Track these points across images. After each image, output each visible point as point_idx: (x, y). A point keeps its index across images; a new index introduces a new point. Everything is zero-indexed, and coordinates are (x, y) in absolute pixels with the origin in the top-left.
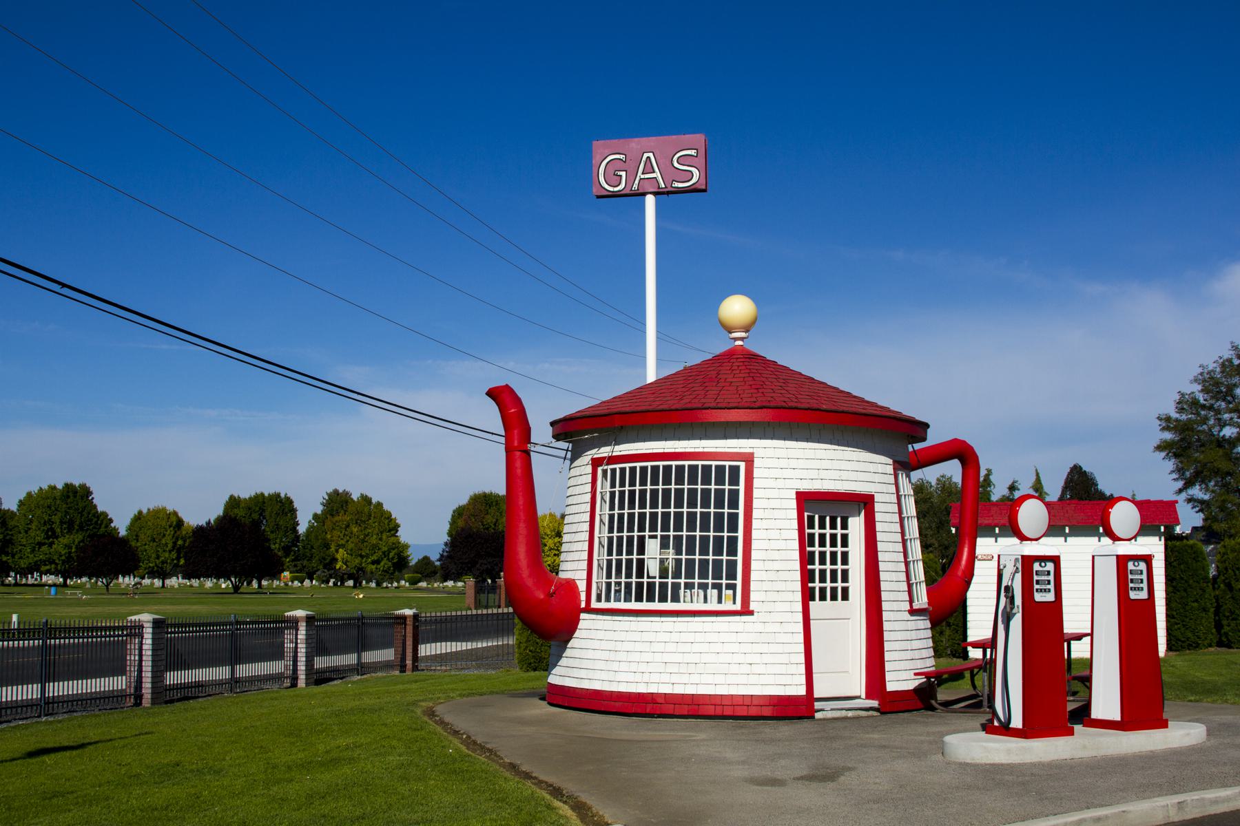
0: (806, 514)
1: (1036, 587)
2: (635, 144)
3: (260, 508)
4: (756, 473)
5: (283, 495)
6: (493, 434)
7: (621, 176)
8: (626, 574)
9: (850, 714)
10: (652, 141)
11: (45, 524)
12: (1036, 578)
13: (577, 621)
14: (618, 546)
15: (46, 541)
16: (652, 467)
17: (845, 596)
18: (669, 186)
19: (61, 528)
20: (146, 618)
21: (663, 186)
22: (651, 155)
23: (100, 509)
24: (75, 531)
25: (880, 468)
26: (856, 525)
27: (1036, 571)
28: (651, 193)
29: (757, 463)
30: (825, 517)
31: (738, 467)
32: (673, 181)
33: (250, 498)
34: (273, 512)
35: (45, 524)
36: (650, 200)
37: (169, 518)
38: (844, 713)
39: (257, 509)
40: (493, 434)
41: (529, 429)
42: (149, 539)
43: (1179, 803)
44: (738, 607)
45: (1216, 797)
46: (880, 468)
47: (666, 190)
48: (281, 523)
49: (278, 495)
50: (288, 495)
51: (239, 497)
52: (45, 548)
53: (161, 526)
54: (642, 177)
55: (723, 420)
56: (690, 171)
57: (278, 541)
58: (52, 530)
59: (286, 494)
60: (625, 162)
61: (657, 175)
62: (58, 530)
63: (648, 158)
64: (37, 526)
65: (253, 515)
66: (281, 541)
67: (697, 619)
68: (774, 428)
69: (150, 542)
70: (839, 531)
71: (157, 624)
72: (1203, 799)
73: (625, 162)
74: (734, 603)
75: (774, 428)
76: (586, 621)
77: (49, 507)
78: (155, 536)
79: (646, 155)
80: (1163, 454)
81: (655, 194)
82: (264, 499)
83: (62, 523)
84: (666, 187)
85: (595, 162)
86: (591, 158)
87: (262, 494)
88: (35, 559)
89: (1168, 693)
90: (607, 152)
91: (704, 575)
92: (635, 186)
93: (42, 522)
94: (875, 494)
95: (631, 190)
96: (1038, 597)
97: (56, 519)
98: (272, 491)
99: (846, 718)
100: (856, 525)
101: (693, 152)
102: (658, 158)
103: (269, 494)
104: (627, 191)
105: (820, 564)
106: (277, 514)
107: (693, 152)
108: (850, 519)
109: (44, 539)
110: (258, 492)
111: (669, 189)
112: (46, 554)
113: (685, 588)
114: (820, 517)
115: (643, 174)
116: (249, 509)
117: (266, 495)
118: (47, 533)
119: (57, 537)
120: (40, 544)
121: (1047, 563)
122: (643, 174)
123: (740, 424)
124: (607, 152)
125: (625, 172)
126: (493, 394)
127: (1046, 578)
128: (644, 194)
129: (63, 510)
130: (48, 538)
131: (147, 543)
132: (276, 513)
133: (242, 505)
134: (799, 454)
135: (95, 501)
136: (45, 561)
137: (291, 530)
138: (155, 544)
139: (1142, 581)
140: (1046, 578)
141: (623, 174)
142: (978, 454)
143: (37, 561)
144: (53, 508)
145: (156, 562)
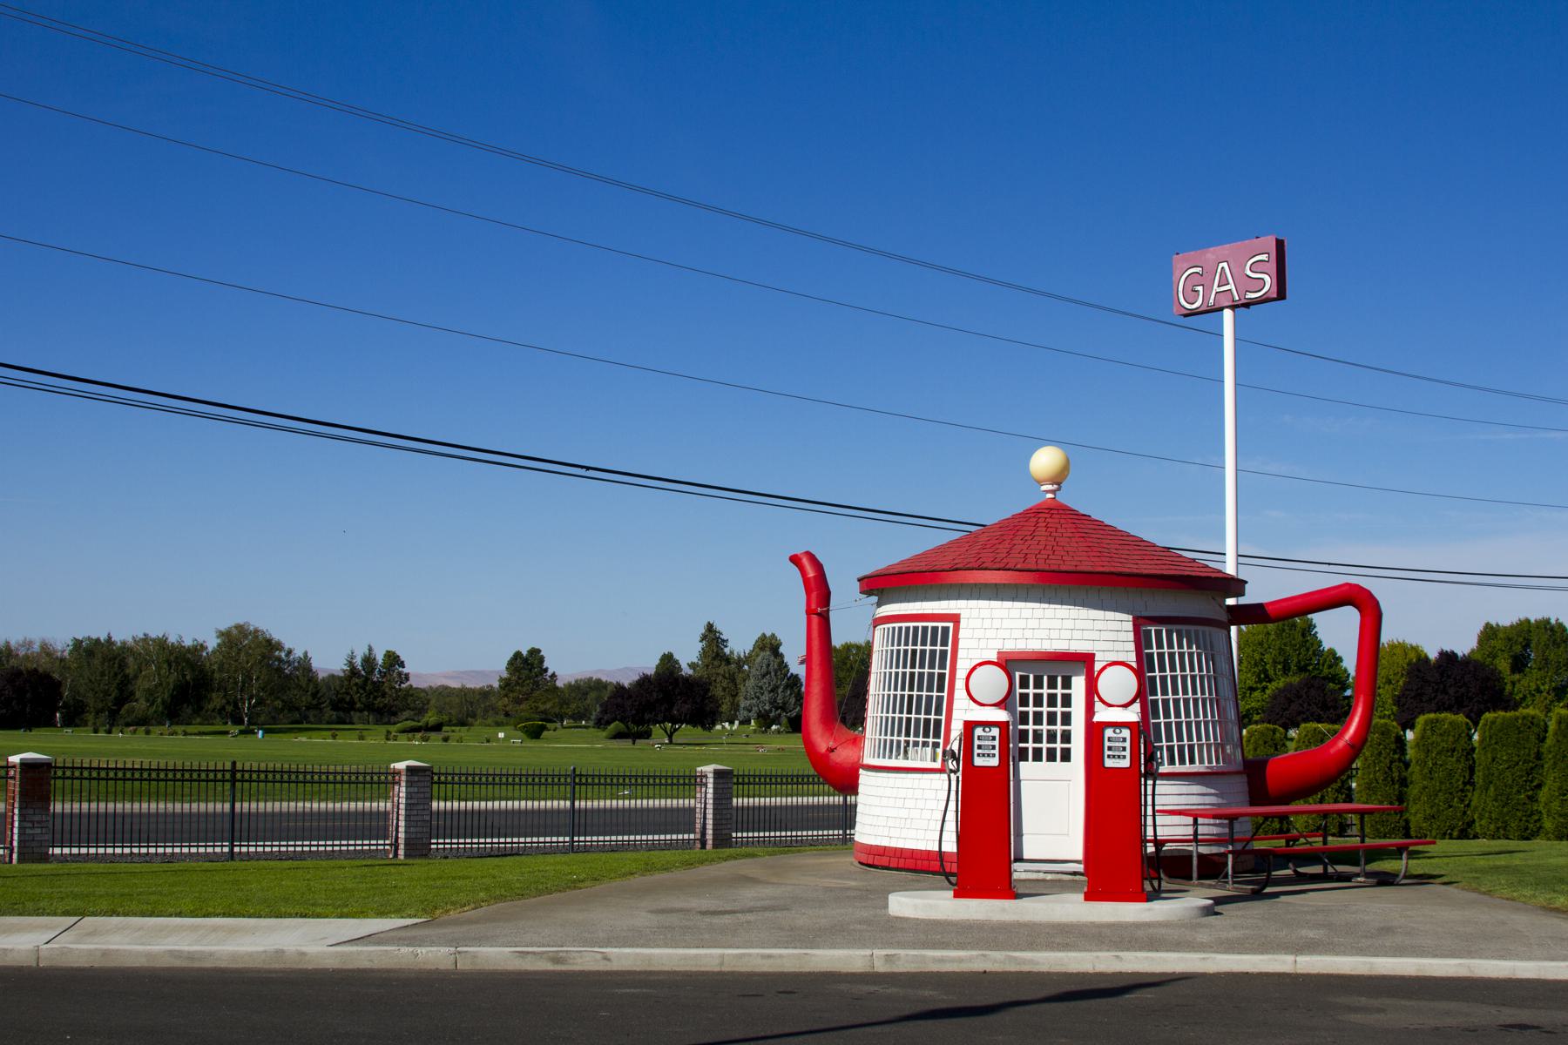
0: (1017, 674)
1: (1107, 752)
2: (1210, 255)
3: (1524, 639)
4: (962, 634)
5: (1553, 621)
6: (1329, 564)
7: (1198, 291)
8: (923, 733)
9: (1049, 877)
10: (1225, 249)
11: (1256, 665)
12: (1107, 744)
13: (857, 777)
14: (926, 704)
15: (1258, 685)
16: (943, 627)
17: (1066, 756)
18: (1242, 298)
19: (1275, 670)
20: (709, 769)
21: (1237, 299)
22: (1225, 265)
23: (1326, 646)
24: (1291, 673)
25: (1117, 626)
26: (1079, 684)
27: (979, 737)
28: (1227, 307)
29: (963, 623)
30: (1056, 677)
31: (948, 628)
32: (1247, 291)
33: (1512, 626)
34: (1540, 643)
35: (1256, 665)
36: (1228, 314)
37: (1406, 654)
38: (1041, 876)
39: (1521, 639)
40: (1329, 564)
41: (829, 593)
42: (1384, 680)
43: (887, 955)
44: (938, 765)
45: (942, 956)
46: (1117, 626)
47: (1241, 302)
48: (1552, 657)
49: (1548, 621)
50: (1560, 621)
51: (1497, 625)
52: (1257, 694)
53: (1398, 664)
54: (1218, 290)
55: (972, 582)
56: (1263, 279)
57: (1547, 680)
58: (1265, 671)
59: (1558, 620)
60: (1202, 275)
61: (1231, 286)
62: (1271, 672)
63: (1223, 268)
64: (1247, 668)
65: (1514, 648)
66: (1551, 681)
67: (910, 776)
68: (980, 589)
69: (1384, 684)
70: (1059, 691)
71: (717, 774)
72: (924, 956)
73: (1202, 275)
74: (934, 761)
75: (980, 589)
76: (865, 778)
77: (1261, 644)
78: (1391, 677)
79: (1221, 265)
80: (358, 661)
81: (1233, 307)
82: (1530, 627)
83: (1275, 662)
84: (1240, 300)
85: (1175, 279)
86: (1171, 274)
87: (1528, 621)
88: (1247, 707)
89: (955, 859)
90: (1186, 265)
91: (926, 735)
92: (1212, 301)
93: (1253, 662)
94: (1096, 653)
95: (1233, 301)
96: (978, 762)
97: (1267, 658)
98: (1539, 617)
99: (1044, 880)
100: (1079, 684)
101: (1264, 257)
102: (1233, 271)
103: (1536, 621)
104: (1204, 308)
105: (1063, 724)
106: (1547, 646)
107: (1264, 257)
108: (1073, 679)
109: (1256, 682)
110: (1522, 618)
111: (1244, 301)
112: (1258, 701)
113: (914, 746)
114: (1035, 677)
115: (1219, 286)
116: (1510, 640)
117: (1533, 621)
118: (1259, 676)
119: (1270, 681)
120: (1252, 689)
121: (1123, 730)
122: (1219, 286)
123: (986, 585)
124: (1186, 265)
125: (1201, 287)
126: (795, 560)
127: (1121, 744)
128: (1221, 309)
129: (1277, 647)
130: (1260, 681)
131: (1382, 686)
132: (1545, 645)
133: (1501, 635)
134: (1004, 613)
135: (1320, 636)
136: (1257, 710)
137: (1564, 665)
138: (1391, 686)
139: (1124, 749)
140: (1121, 744)
141: (1200, 288)
142: (1378, 599)
143: (1248, 710)
144: (1266, 646)
145: (1392, 709)
